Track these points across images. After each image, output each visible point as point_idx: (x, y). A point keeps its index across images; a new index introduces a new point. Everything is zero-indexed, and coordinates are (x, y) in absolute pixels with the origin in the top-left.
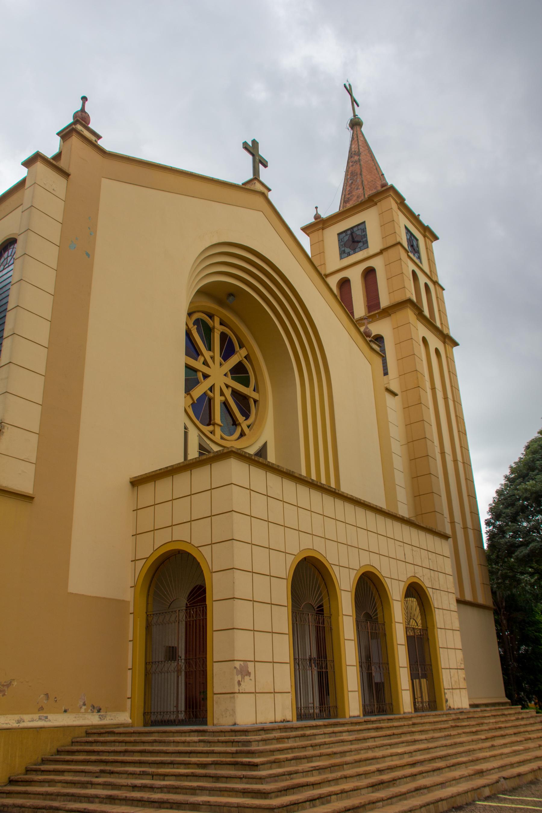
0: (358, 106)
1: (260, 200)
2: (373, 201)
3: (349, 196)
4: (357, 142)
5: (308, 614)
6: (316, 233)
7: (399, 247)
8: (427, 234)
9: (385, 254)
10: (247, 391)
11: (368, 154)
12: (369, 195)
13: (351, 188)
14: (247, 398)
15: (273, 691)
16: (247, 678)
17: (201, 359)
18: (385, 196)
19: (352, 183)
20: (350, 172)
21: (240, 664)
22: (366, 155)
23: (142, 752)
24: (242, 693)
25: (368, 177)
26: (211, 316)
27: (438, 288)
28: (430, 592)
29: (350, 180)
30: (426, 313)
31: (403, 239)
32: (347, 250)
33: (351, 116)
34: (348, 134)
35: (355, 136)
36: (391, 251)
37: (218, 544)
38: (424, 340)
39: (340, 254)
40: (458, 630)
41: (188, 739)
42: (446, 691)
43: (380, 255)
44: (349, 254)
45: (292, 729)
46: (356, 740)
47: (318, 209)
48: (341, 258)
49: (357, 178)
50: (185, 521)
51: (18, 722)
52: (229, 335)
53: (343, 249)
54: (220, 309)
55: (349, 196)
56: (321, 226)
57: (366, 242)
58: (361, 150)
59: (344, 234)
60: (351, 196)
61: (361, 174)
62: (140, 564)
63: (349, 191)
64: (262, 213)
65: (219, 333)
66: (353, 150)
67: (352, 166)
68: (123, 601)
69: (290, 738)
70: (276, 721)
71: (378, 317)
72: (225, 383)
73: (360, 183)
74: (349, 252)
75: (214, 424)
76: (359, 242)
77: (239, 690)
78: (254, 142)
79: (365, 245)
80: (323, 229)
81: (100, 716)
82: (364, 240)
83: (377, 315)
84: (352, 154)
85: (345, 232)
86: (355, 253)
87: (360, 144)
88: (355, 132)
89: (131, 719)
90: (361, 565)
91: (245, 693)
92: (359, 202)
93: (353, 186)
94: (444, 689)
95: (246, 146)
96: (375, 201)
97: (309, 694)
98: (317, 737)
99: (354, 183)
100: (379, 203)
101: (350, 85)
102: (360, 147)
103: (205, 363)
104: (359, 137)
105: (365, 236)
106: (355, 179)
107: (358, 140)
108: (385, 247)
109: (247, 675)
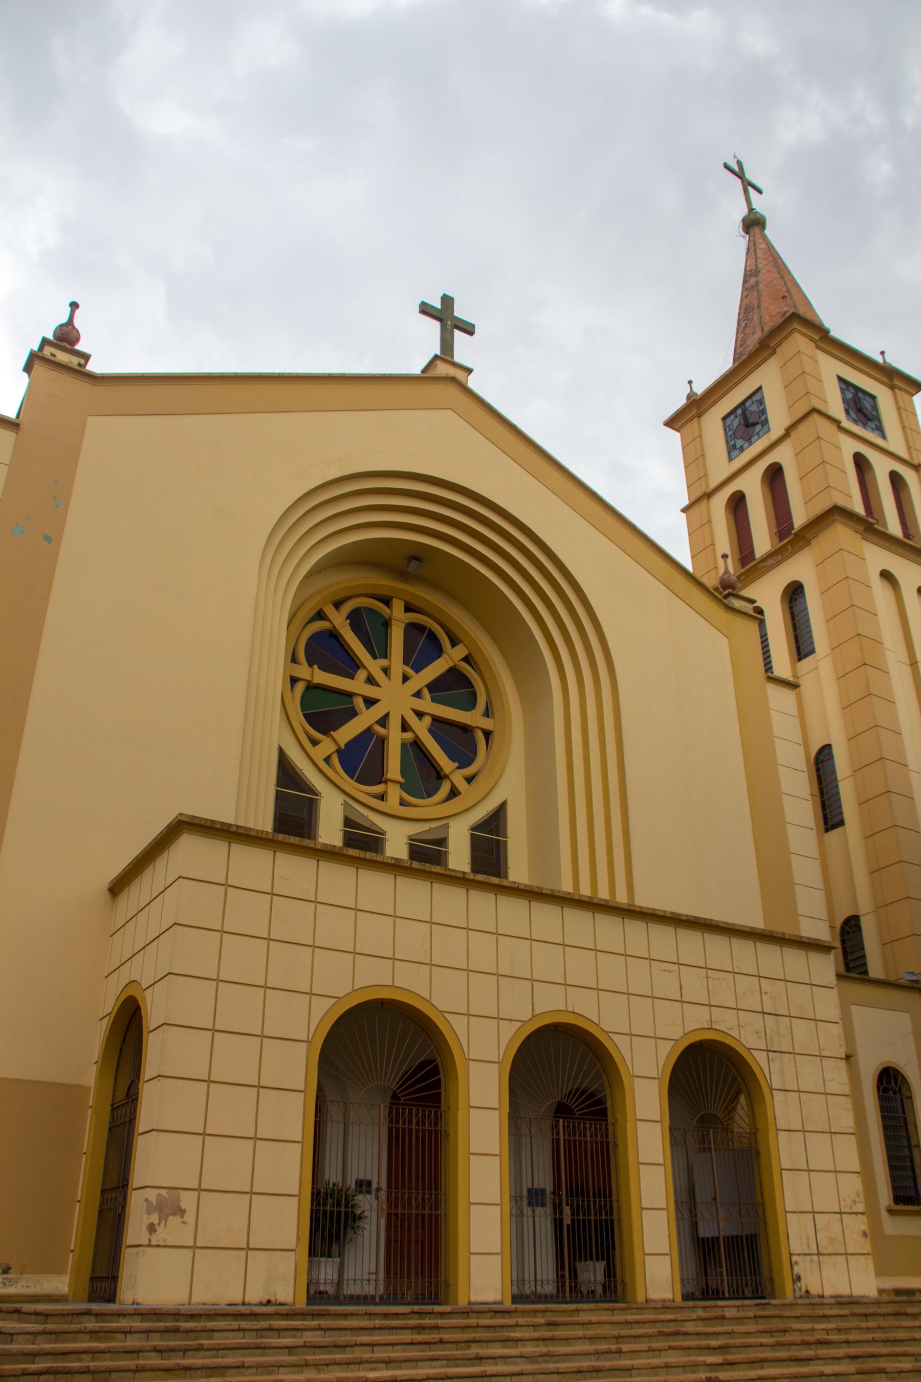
0: (760, 192)
1: (452, 391)
2: (769, 346)
3: (742, 349)
5: (380, 1106)
6: (689, 425)
7: (815, 416)
8: (896, 382)
9: (793, 434)
10: (472, 718)
11: (773, 270)
13: (745, 334)
14: (469, 729)
15: (244, 1246)
16: (174, 1221)
17: (362, 675)
18: (790, 330)
19: (746, 325)
21: (159, 1194)
22: (769, 271)
23: (752, 1363)
24: (158, 1246)
25: (772, 307)
26: (387, 601)
28: (759, 1060)
29: (744, 320)
30: (894, 528)
31: (829, 400)
32: (739, 443)
33: (744, 211)
34: (741, 243)
36: (802, 427)
38: (886, 575)
39: (729, 453)
40: (853, 1134)
42: (794, 1258)
43: (786, 439)
44: (742, 449)
45: (177, 1317)
46: (305, 1346)
47: (693, 385)
48: (730, 459)
49: (753, 316)
52: (429, 626)
53: (733, 442)
54: (401, 586)
55: (742, 349)
56: (695, 411)
57: (766, 422)
58: (760, 266)
59: (732, 417)
60: (745, 348)
61: (759, 307)
63: (741, 340)
64: (451, 410)
65: (403, 626)
68: (78, 1086)
69: (130, 1332)
70: (247, 1301)
71: (790, 550)
72: (412, 709)
73: (757, 323)
74: (742, 447)
75: (386, 782)
76: (756, 424)
77: (150, 1240)
78: (447, 301)
79: (766, 427)
80: (699, 416)
81: (5, 1280)
82: (763, 418)
83: (789, 547)
84: (750, 275)
85: (733, 412)
86: (750, 444)
87: (759, 255)
88: (752, 239)
91: (166, 1246)
92: (747, 355)
93: (747, 331)
94: (791, 1254)
95: (425, 310)
96: (772, 346)
97: (526, 1257)
98: (215, 1334)
99: (748, 325)
100: (779, 347)
101: (739, 163)
103: (371, 680)
104: (757, 244)
105: (764, 412)
106: (750, 317)
108: (795, 419)
109: (174, 1214)
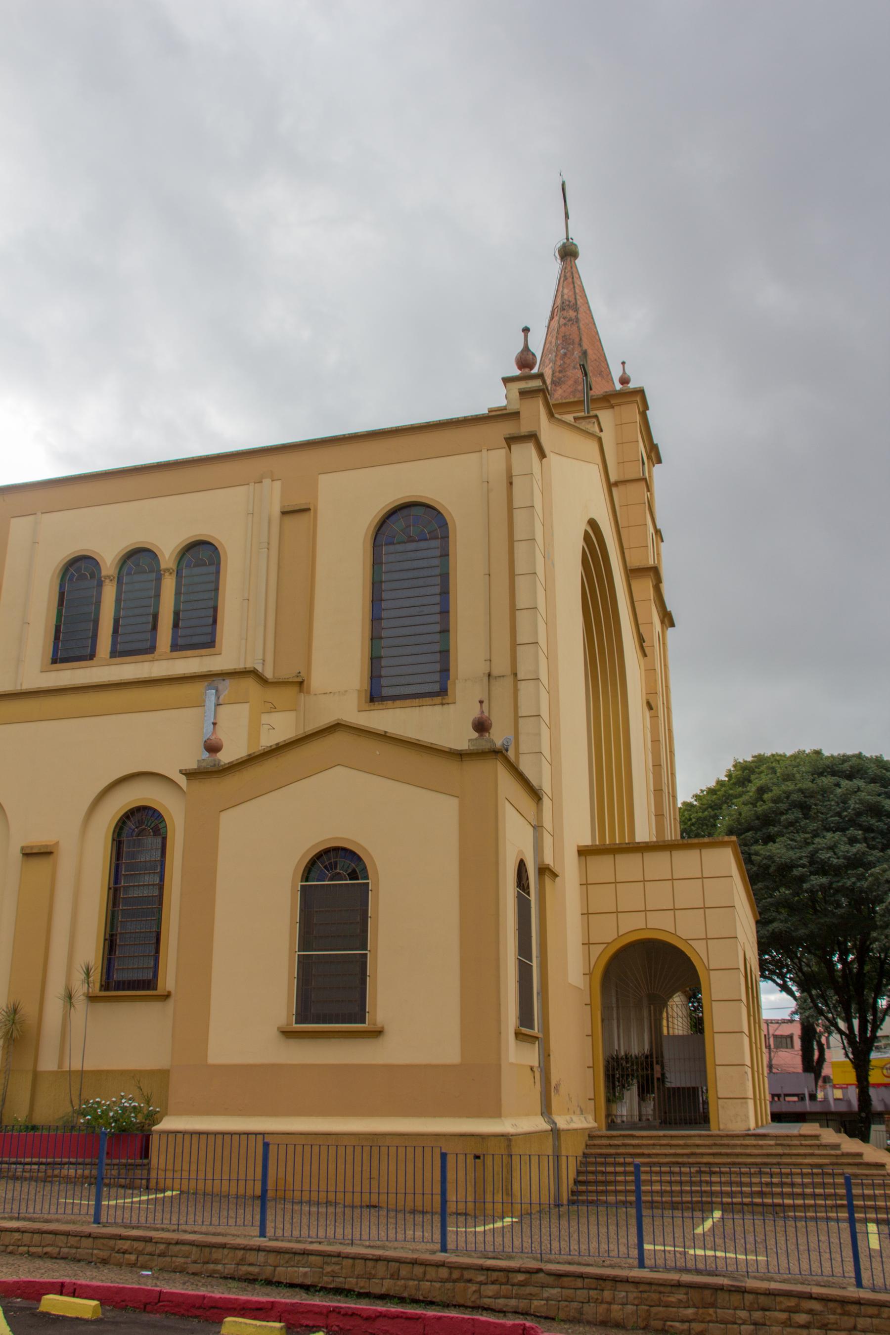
2: (609, 402)
3: (560, 375)
4: (572, 286)
12: (606, 392)
20: (561, 334)
27: (659, 540)
34: (556, 266)
35: (568, 275)
37: (716, 940)
41: (616, 1142)
49: (573, 349)
50: (665, 908)
51: (568, 1123)
58: (578, 302)
60: (564, 376)
62: (596, 951)
66: (566, 297)
67: (565, 325)
89: (596, 1121)
90: (620, 935)
96: (612, 402)
102: (578, 297)
106: (570, 349)
107: (573, 283)
